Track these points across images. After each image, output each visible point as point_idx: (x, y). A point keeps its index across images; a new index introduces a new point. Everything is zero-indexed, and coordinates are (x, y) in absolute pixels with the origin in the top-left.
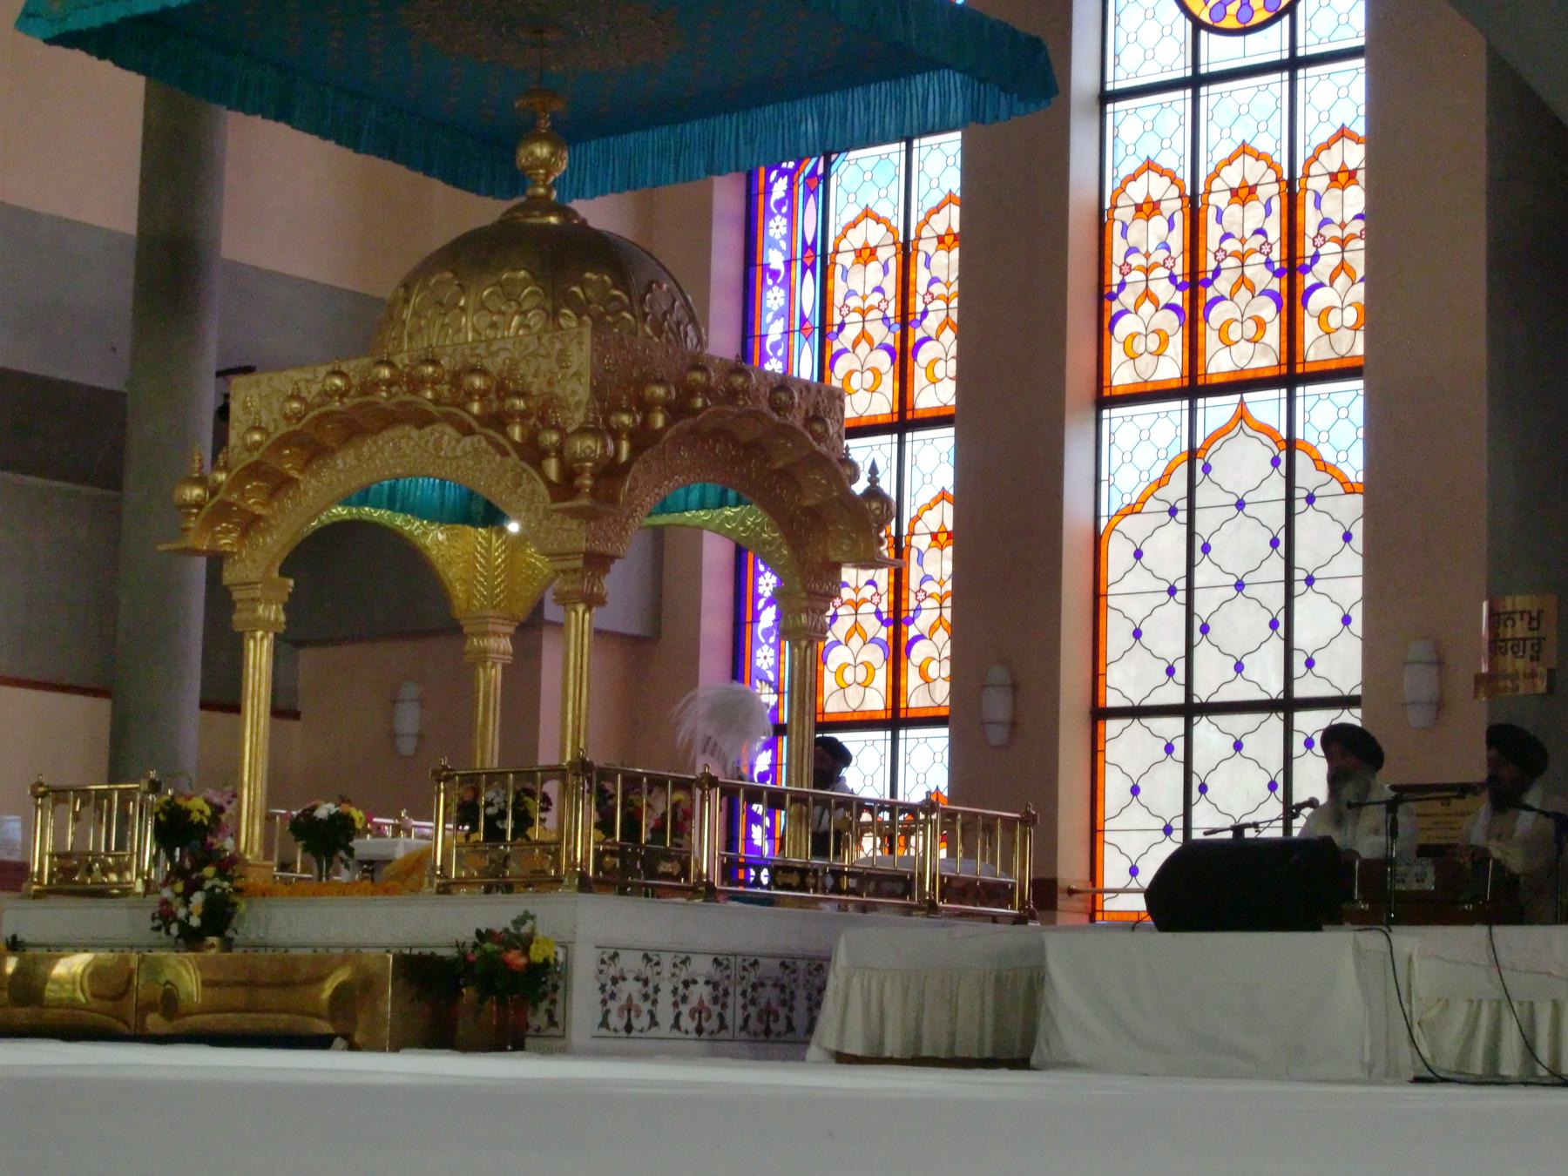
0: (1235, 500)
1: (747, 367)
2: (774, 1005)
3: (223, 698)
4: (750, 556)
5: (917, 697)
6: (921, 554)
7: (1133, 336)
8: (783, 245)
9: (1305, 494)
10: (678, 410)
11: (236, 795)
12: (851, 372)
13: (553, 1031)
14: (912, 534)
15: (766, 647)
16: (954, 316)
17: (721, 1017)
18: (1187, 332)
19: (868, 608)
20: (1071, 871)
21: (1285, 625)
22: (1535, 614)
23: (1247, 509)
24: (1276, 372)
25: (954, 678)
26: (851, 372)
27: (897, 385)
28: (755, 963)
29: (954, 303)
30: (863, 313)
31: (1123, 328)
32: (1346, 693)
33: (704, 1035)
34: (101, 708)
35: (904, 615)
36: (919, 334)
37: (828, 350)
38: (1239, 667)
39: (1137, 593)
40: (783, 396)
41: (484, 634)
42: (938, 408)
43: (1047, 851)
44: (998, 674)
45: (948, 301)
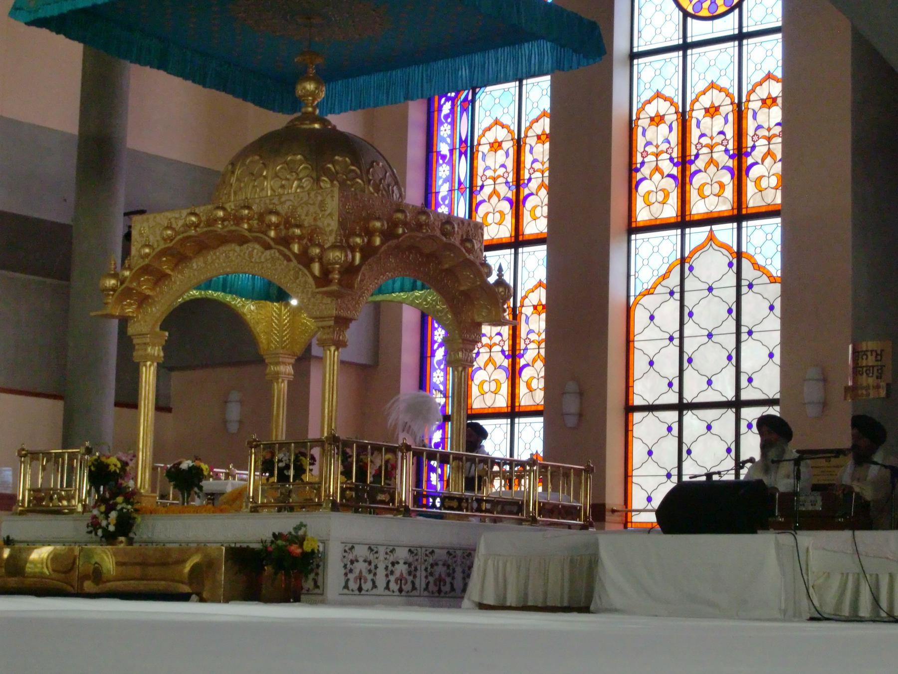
0: (707, 287)
1: (428, 210)
2: (443, 576)
3: (128, 400)
4: (430, 319)
5: (525, 400)
6: (527, 318)
7: (649, 193)
8: (449, 140)
9: (747, 283)
10: (388, 235)
11: (135, 456)
12: (487, 213)
13: (317, 591)
14: (522, 306)
15: (438, 371)
16: (546, 181)
17: (413, 583)
18: (680, 190)
19: (497, 349)
20: (613, 499)
21: (736, 358)
22: (879, 352)
23: (714, 292)
24: (731, 213)
25: (546, 389)
26: (487, 213)
27: (514, 221)
28: (433, 552)
29: (547, 174)
30: (494, 179)
31: (643, 188)
32: (771, 397)
33: (403, 593)
34: (58, 406)
35: (517, 352)
36: (526, 191)
37: (474, 200)
38: (710, 382)
39: (651, 340)
40: (448, 227)
41: (277, 363)
42: (537, 234)
43: (600, 487)
44: (571, 386)
45: (543, 172)
